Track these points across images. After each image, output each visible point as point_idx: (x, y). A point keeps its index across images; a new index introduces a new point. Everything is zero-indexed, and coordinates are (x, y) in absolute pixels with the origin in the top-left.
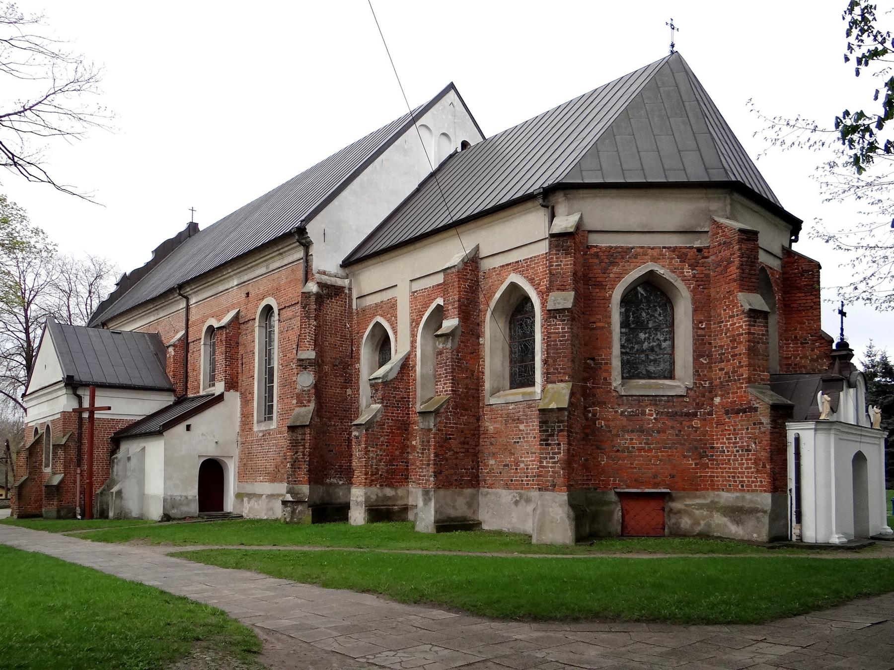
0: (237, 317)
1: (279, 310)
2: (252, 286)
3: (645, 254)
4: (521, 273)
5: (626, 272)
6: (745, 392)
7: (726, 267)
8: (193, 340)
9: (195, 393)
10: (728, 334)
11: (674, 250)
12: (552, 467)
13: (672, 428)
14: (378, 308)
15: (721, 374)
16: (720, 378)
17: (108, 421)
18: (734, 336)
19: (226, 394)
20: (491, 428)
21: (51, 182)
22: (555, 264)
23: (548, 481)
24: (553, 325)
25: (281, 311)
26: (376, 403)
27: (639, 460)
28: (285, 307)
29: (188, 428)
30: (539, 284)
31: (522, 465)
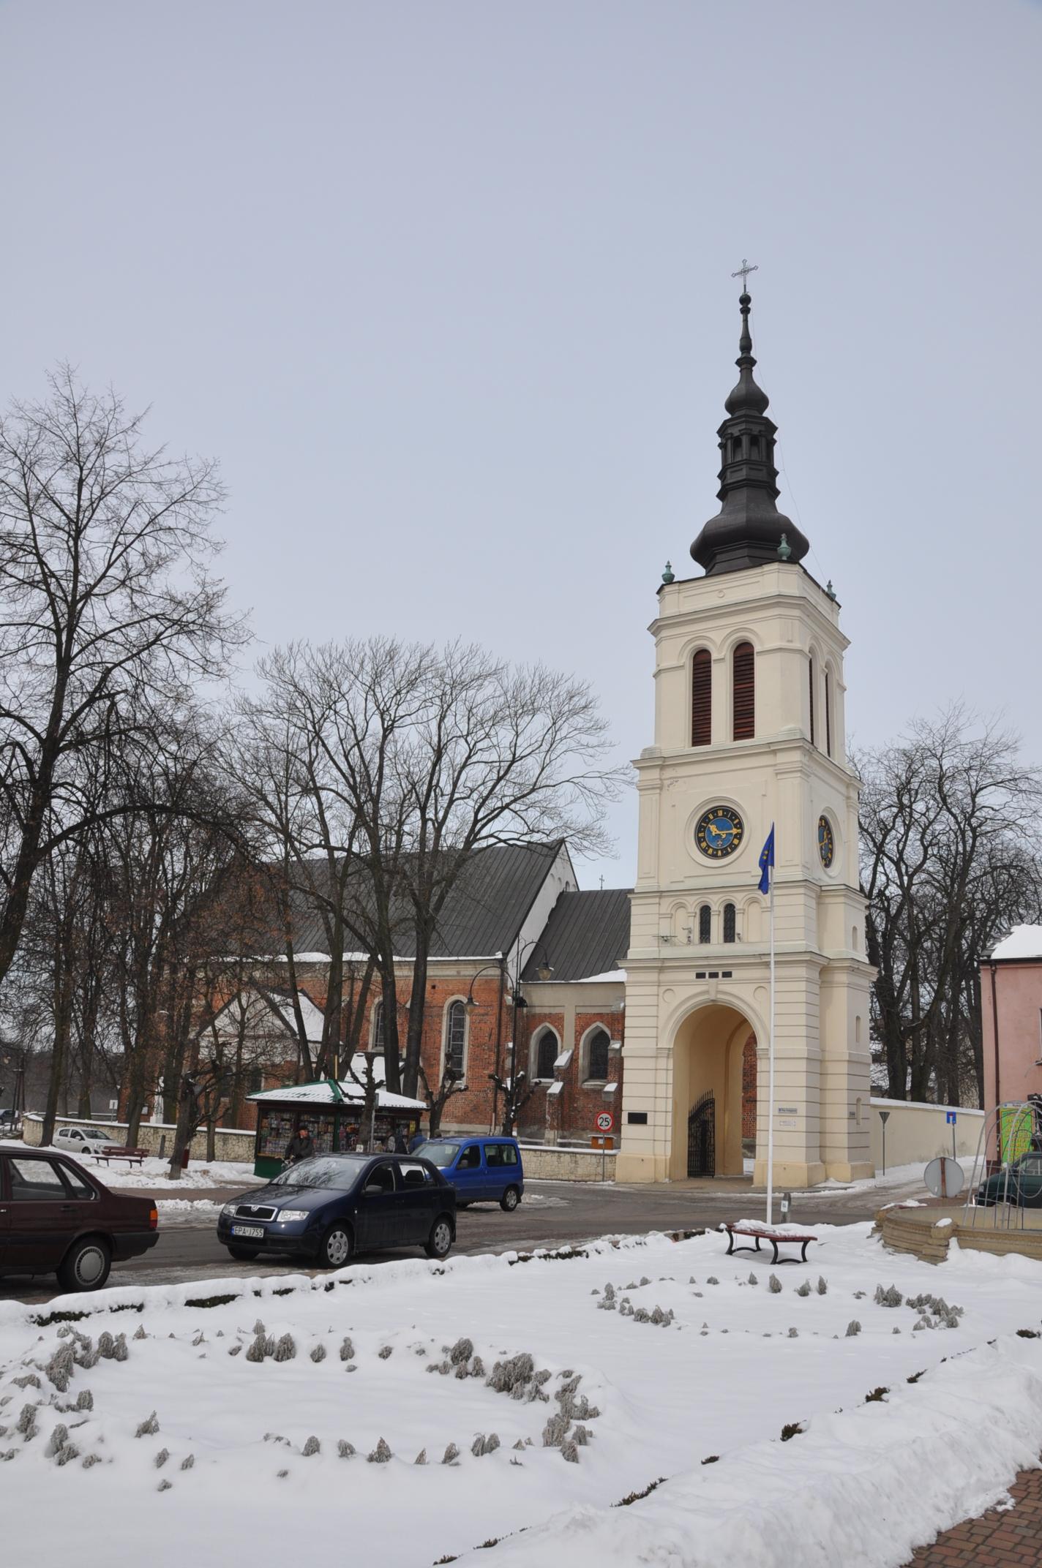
14: (549, 1017)
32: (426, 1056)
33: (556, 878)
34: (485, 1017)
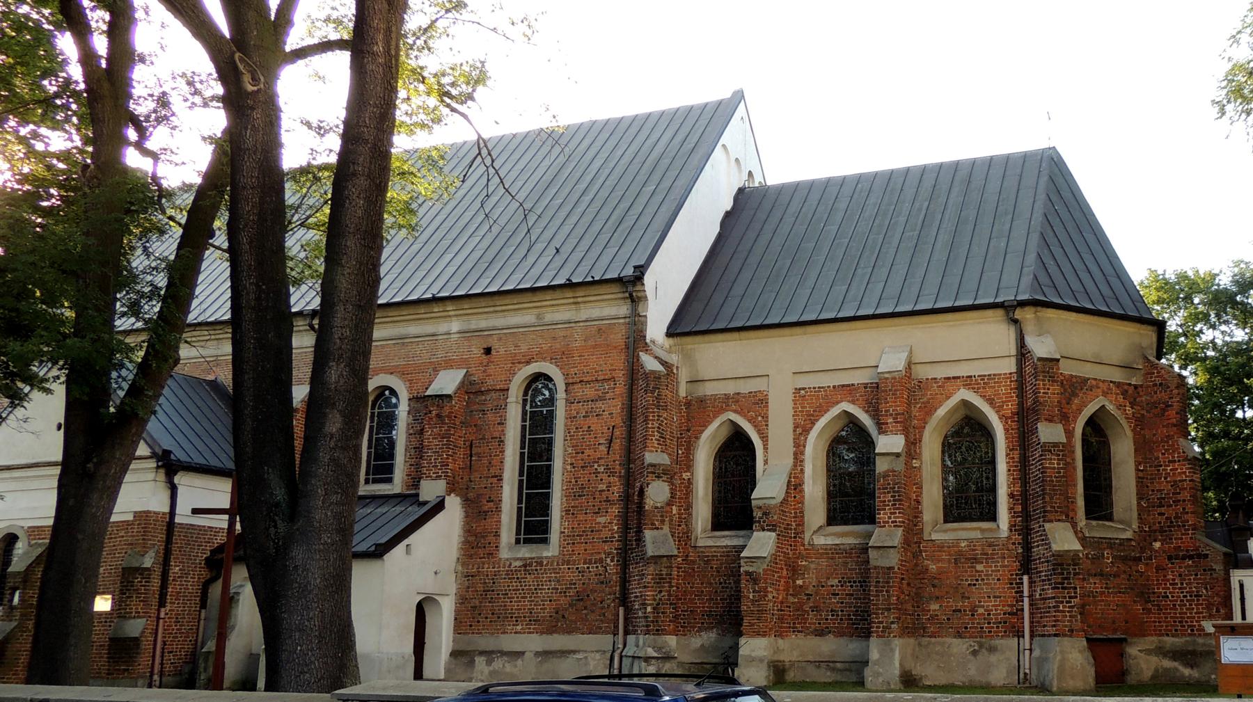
1: (567, 384)
2: (500, 339)
5: (1084, 404)
6: (1191, 538)
7: (1164, 410)
10: (1169, 479)
11: (1118, 385)
12: (1068, 612)
13: (1125, 572)
14: (727, 402)
15: (1162, 519)
16: (1160, 523)
17: (204, 531)
18: (1175, 481)
19: (447, 499)
22: (1042, 391)
23: (1066, 626)
25: (571, 387)
26: (764, 530)
27: (1101, 605)
28: (581, 381)
31: (981, 611)
32: (471, 495)
33: (733, 160)
34: (599, 404)
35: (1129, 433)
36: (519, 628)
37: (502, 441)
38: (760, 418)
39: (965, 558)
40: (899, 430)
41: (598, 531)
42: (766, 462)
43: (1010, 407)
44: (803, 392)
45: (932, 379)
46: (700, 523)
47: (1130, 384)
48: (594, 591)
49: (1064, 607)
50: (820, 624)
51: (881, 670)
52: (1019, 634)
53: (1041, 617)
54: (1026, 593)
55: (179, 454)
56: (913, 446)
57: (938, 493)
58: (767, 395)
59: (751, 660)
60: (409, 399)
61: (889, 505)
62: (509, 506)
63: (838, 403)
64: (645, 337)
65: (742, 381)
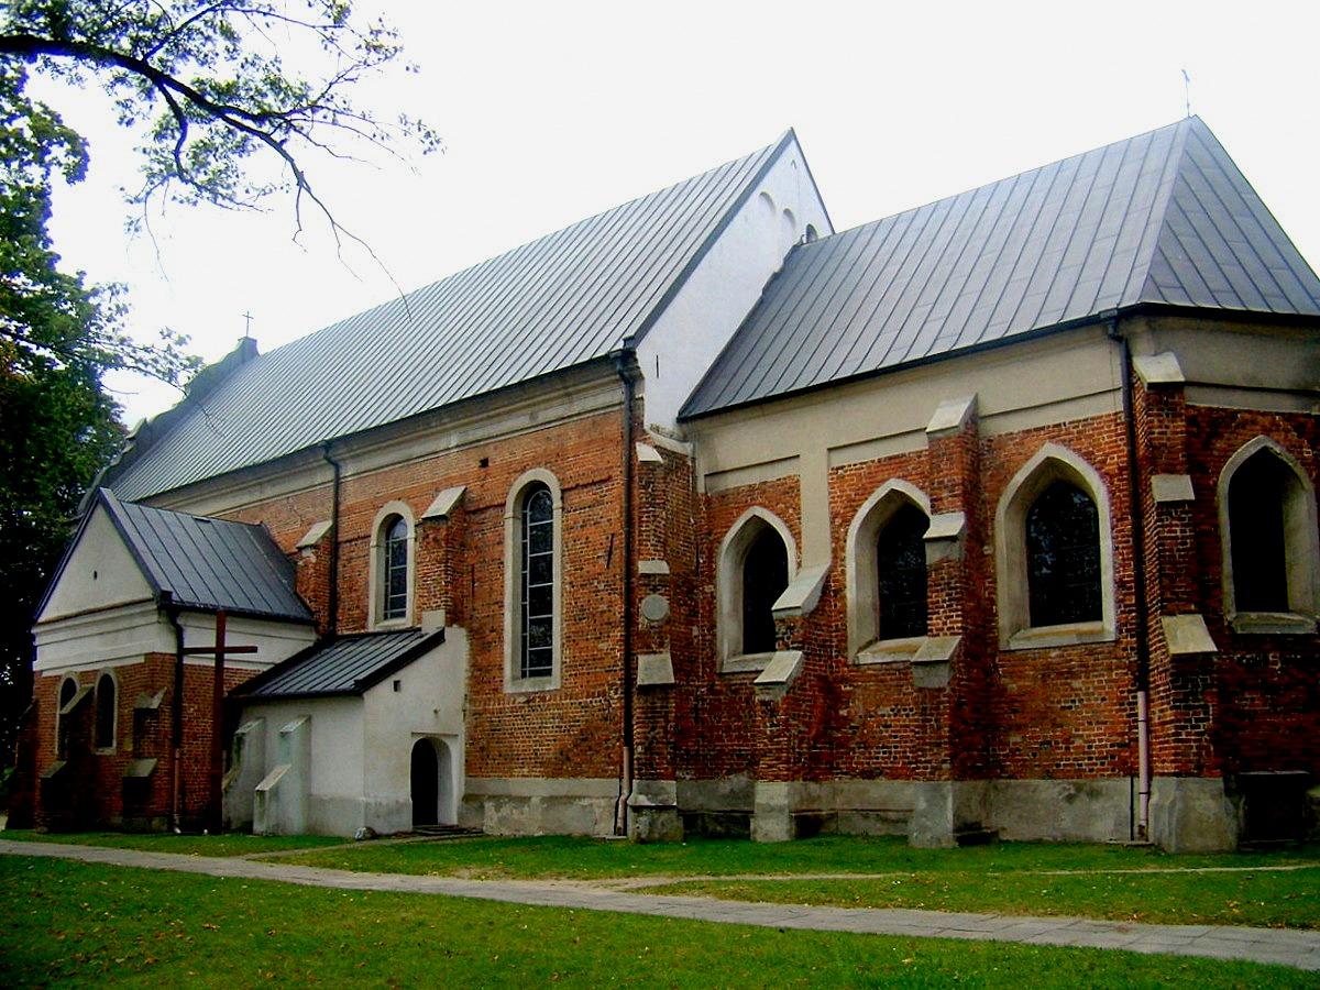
0: (461, 501)
1: (563, 491)
2: (496, 448)
3: (1254, 422)
4: (1067, 443)
5: (1232, 448)
8: (351, 537)
9: (355, 629)
11: (1288, 417)
12: (1195, 741)
14: (753, 494)
19: (448, 632)
20: (1013, 687)
21: (333, 223)
22: (1157, 431)
24: (1167, 526)
25: (566, 495)
26: (788, 649)
28: (577, 485)
29: (397, 685)
30: (1104, 462)
31: (1078, 742)
32: (476, 625)
35: (1308, 484)
36: (525, 770)
37: (502, 563)
38: (791, 511)
39: (1057, 671)
40: (958, 507)
41: (600, 659)
42: (799, 565)
43: (1117, 460)
44: (840, 471)
45: (1007, 435)
46: (726, 646)
47: (1309, 416)
48: (597, 729)
49: (1188, 734)
50: (868, 763)
51: (928, 823)
52: (1133, 773)
53: (1161, 749)
54: (1141, 717)
55: (183, 594)
56: (977, 532)
57: (1022, 587)
58: (798, 481)
59: (771, 810)
60: (416, 526)
61: (943, 607)
62: (510, 636)
63: (884, 481)
64: (642, 423)
65: (769, 467)
